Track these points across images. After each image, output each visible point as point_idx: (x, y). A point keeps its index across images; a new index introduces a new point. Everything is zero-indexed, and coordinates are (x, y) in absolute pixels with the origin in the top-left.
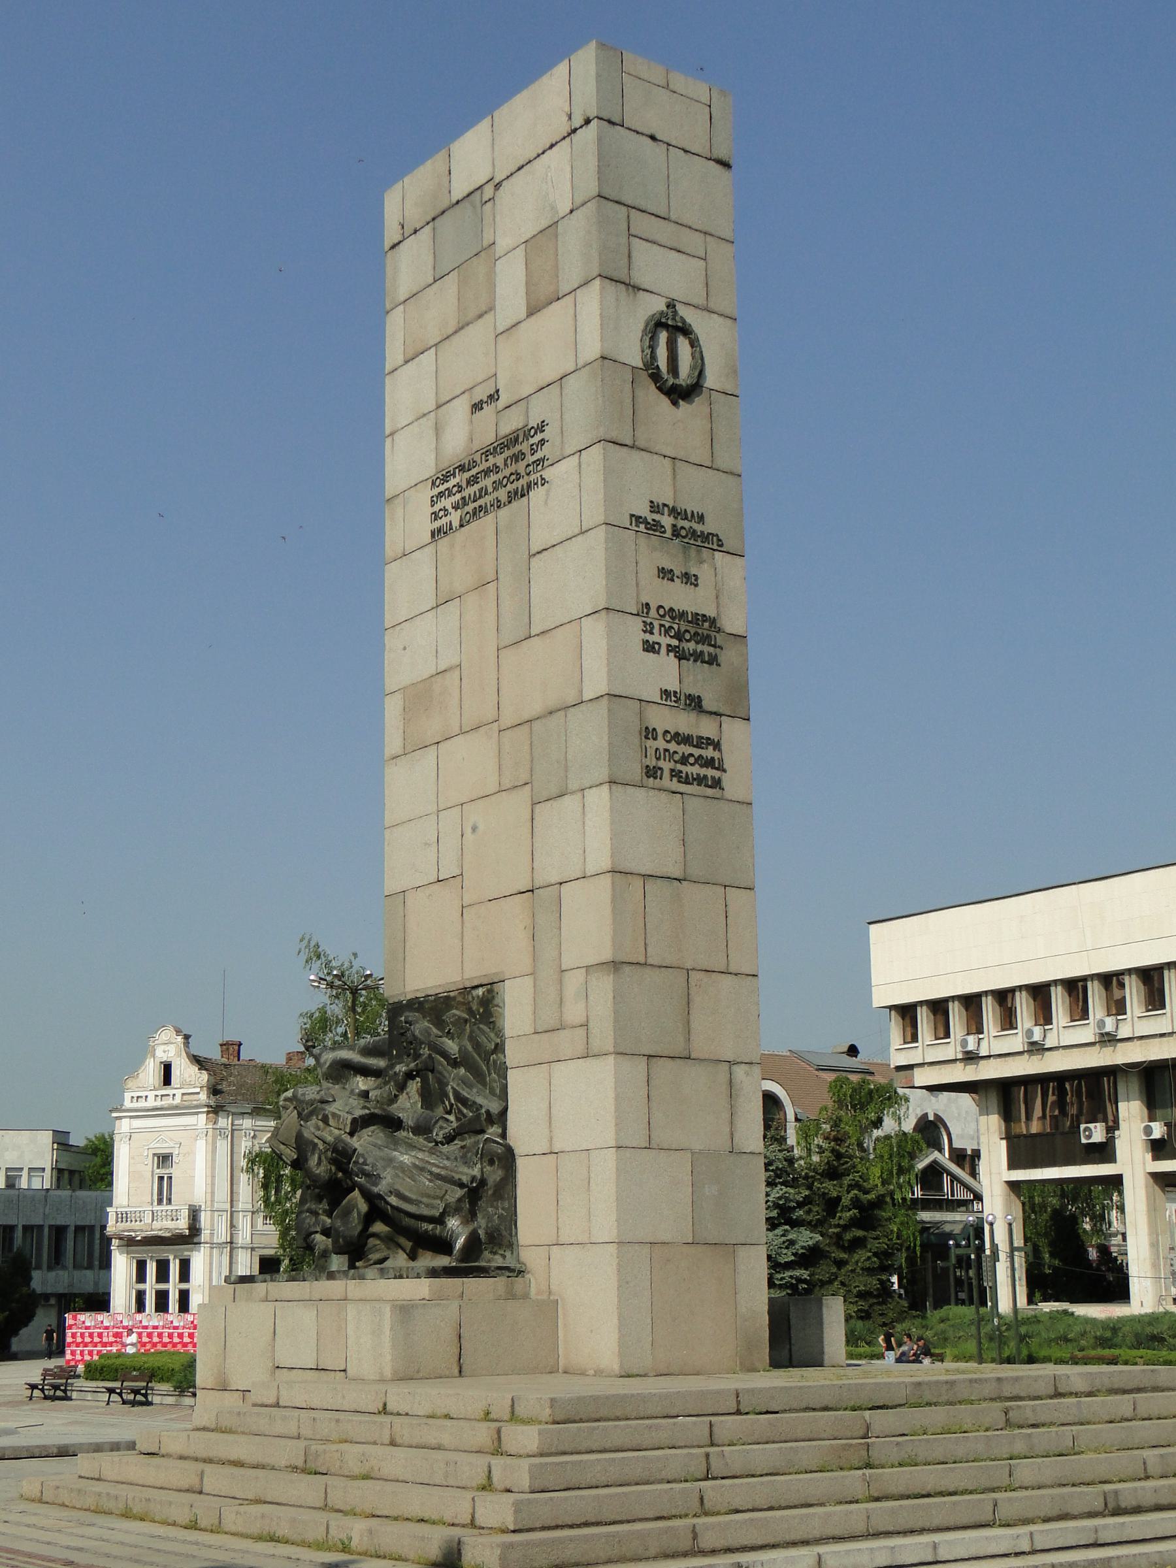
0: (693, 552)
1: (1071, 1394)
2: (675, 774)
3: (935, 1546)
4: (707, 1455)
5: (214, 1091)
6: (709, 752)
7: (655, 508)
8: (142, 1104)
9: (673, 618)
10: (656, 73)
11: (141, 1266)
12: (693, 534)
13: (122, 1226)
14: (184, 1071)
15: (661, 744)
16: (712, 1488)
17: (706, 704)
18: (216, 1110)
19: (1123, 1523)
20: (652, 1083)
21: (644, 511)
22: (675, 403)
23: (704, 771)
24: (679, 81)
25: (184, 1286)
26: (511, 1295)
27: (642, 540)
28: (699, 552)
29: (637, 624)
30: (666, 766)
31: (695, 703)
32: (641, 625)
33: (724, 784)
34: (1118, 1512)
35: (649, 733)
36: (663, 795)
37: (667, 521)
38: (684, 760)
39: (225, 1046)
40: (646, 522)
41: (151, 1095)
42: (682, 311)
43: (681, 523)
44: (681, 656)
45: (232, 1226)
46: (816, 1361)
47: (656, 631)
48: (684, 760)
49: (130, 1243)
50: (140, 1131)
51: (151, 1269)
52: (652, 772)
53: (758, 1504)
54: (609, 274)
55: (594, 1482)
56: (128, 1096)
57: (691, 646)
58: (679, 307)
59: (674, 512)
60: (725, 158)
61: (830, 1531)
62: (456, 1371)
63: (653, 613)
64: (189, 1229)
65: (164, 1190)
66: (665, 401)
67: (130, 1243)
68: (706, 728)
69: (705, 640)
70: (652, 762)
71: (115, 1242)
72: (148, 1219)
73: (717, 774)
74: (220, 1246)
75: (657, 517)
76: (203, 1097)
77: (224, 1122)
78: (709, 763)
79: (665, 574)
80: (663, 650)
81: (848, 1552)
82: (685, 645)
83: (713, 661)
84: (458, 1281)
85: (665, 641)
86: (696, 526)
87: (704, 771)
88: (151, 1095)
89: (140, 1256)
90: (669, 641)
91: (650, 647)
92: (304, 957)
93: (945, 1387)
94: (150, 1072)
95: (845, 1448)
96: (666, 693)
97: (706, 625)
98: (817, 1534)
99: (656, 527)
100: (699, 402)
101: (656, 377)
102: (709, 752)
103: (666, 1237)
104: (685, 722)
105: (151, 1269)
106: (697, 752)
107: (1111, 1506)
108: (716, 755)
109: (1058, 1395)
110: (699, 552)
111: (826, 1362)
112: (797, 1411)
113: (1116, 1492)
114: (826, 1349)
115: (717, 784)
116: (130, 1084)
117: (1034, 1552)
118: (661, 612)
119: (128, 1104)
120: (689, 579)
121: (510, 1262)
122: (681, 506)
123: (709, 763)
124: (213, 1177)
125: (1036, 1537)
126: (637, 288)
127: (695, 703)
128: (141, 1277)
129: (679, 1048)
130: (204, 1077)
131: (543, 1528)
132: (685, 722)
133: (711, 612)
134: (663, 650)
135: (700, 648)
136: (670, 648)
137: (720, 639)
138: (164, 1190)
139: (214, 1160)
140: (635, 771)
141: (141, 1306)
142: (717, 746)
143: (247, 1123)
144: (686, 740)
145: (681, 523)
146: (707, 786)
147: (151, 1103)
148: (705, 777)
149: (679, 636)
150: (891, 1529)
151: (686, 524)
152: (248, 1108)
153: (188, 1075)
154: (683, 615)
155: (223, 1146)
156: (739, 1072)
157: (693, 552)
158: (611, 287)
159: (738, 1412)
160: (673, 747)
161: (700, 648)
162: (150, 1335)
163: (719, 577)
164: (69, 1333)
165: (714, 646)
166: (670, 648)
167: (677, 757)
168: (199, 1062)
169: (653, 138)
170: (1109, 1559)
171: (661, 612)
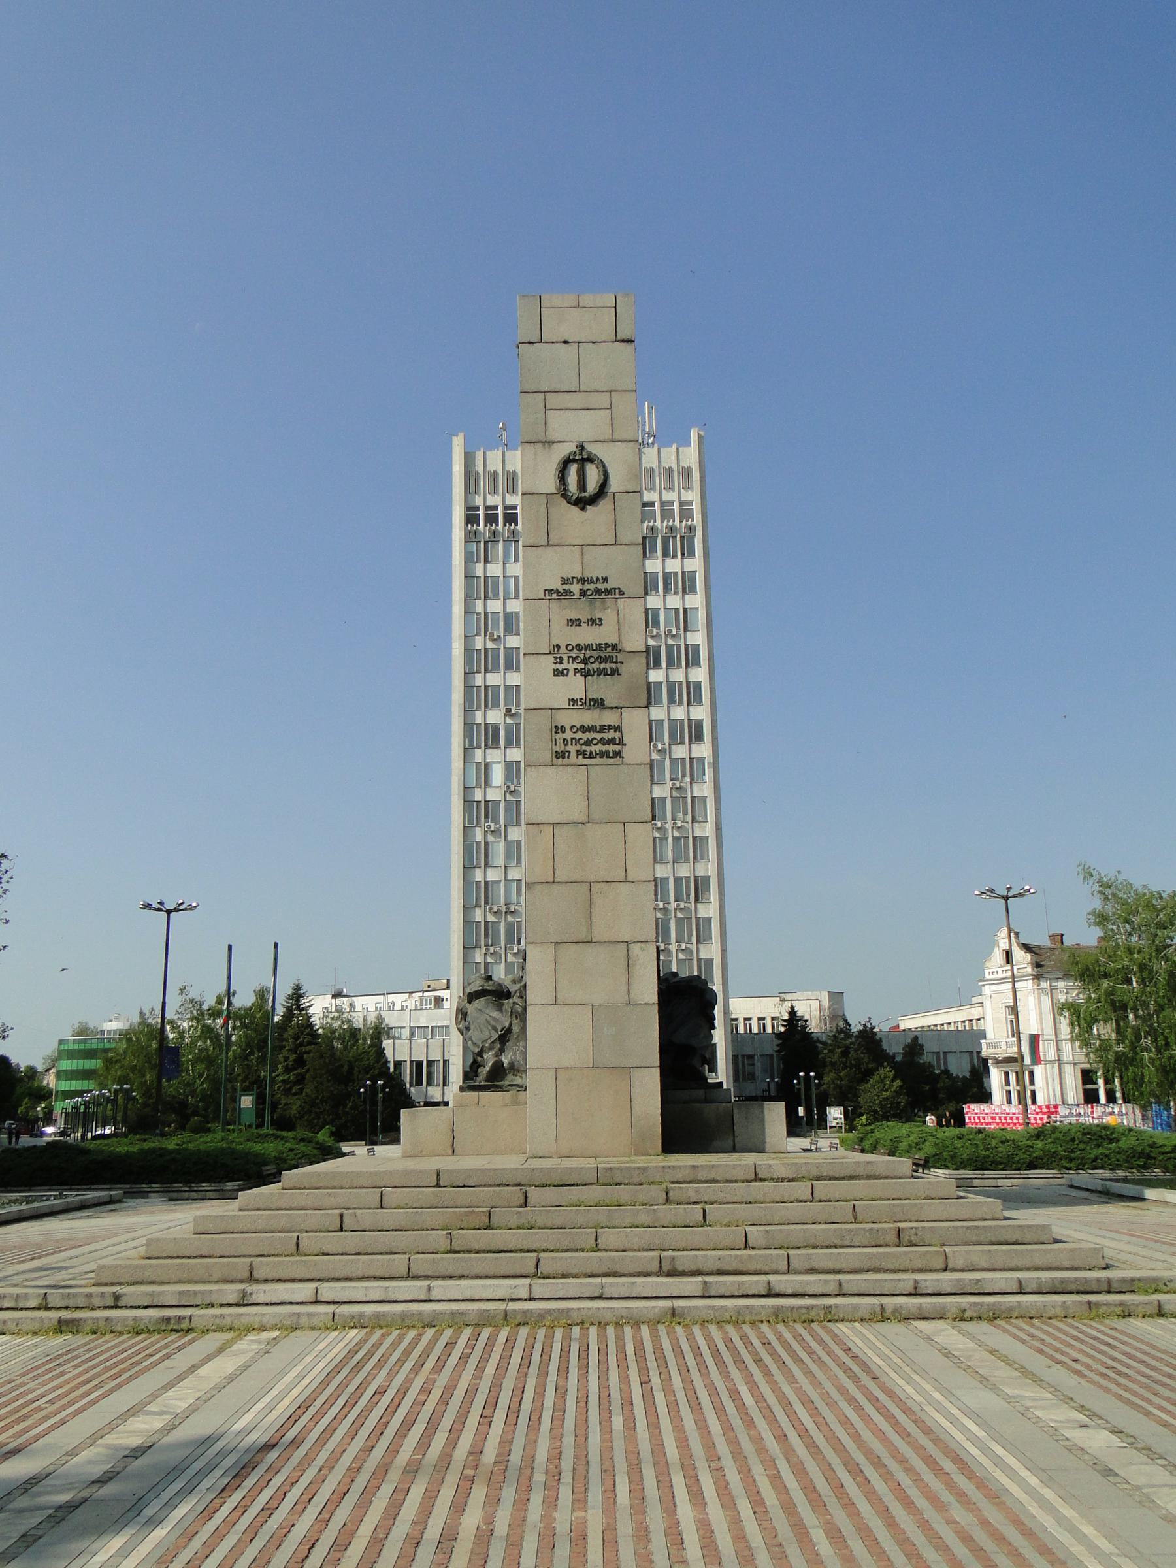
0: (598, 603)
1: (772, 1179)
2: (578, 753)
3: (429, 1289)
4: (341, 1216)
5: (1038, 965)
6: (611, 734)
7: (565, 581)
8: (995, 976)
9: (580, 650)
10: (570, 300)
11: (1007, 1074)
12: (597, 591)
13: (990, 1051)
14: (1019, 955)
15: (568, 735)
16: (309, 1238)
17: (607, 703)
18: (1038, 977)
19: (634, 1283)
20: (558, 960)
21: (556, 585)
22: (583, 509)
23: (604, 748)
24: (587, 300)
25: (1032, 1088)
26: (516, 1103)
27: (554, 605)
28: (603, 603)
29: (551, 659)
30: (573, 749)
31: (599, 704)
32: (553, 660)
33: (624, 754)
34: (672, 1273)
35: (560, 729)
36: (570, 769)
37: (575, 588)
38: (588, 743)
39: (1053, 937)
40: (557, 592)
41: (1000, 970)
42: (590, 448)
43: (587, 586)
44: (586, 674)
45: (1058, 1050)
46: (759, 1148)
47: (565, 661)
48: (588, 743)
49: (998, 1062)
50: (996, 992)
51: (1013, 1077)
52: (560, 755)
53: (347, 1250)
54: (529, 439)
55: (245, 1229)
56: (986, 972)
57: (596, 666)
58: (585, 445)
59: (582, 580)
60: (629, 337)
61: (372, 1273)
62: (450, 1152)
63: (563, 650)
64: (905, 1054)
65: (1015, 1029)
66: (575, 510)
67: (998, 1062)
68: (609, 718)
69: (609, 659)
70: (560, 747)
71: (990, 1061)
72: (1004, 1046)
73: (617, 748)
74: (1052, 1062)
75: (567, 587)
76: (1029, 970)
77: (1044, 984)
78: (611, 741)
79: (576, 622)
80: (571, 673)
81: (342, 1288)
82: (589, 666)
83: (614, 672)
84: (475, 1094)
85: (572, 666)
86: (599, 586)
87: (604, 748)
88: (1000, 970)
89: (1006, 1069)
90: (576, 666)
91: (558, 673)
92: (1081, 877)
93: (637, 1172)
94: (998, 957)
95: (467, 1214)
96: (573, 701)
97: (609, 649)
98: (360, 1274)
99: (568, 593)
100: (604, 505)
101: (565, 495)
102: (611, 734)
103: (572, 1064)
104: (590, 717)
105: (1013, 1077)
106: (599, 736)
107: (665, 1269)
108: (617, 735)
109: (757, 1179)
110: (603, 603)
111: (768, 1147)
112: (490, 1186)
113: (673, 1258)
114: (767, 1140)
115: (617, 754)
116: (988, 964)
117: (531, 1299)
118: (570, 648)
119: (987, 977)
120: (594, 622)
121: (518, 1081)
122: (587, 575)
123: (611, 741)
124: (1041, 1019)
125: (534, 1288)
126: (551, 442)
127: (599, 704)
128: (1008, 1083)
129: (583, 934)
130: (1029, 956)
131: (167, 1257)
132: (590, 717)
133: (613, 640)
134: (571, 673)
135: (603, 666)
136: (576, 671)
137: (620, 657)
138: (1015, 1029)
139: (1040, 1008)
140: (548, 756)
141: (1009, 1101)
142: (617, 729)
143: (1061, 984)
144: (592, 729)
145: (587, 586)
146: (609, 757)
147: (1000, 975)
148: (607, 751)
149: (585, 661)
150: (429, 1273)
151: (592, 587)
152: (1060, 975)
153: (1021, 958)
154: (587, 647)
155: (1046, 1000)
156: (636, 949)
157: (598, 603)
158: (530, 449)
159: (438, 1185)
160: (579, 735)
161: (603, 666)
162: (1011, 1118)
163: (621, 615)
164: (967, 1116)
165: (616, 662)
166: (576, 671)
167: (582, 742)
168: (1027, 948)
169: (566, 342)
170: (568, 1310)
171: (570, 648)
